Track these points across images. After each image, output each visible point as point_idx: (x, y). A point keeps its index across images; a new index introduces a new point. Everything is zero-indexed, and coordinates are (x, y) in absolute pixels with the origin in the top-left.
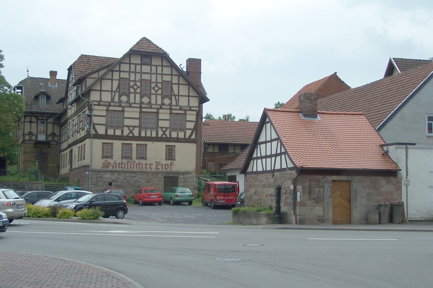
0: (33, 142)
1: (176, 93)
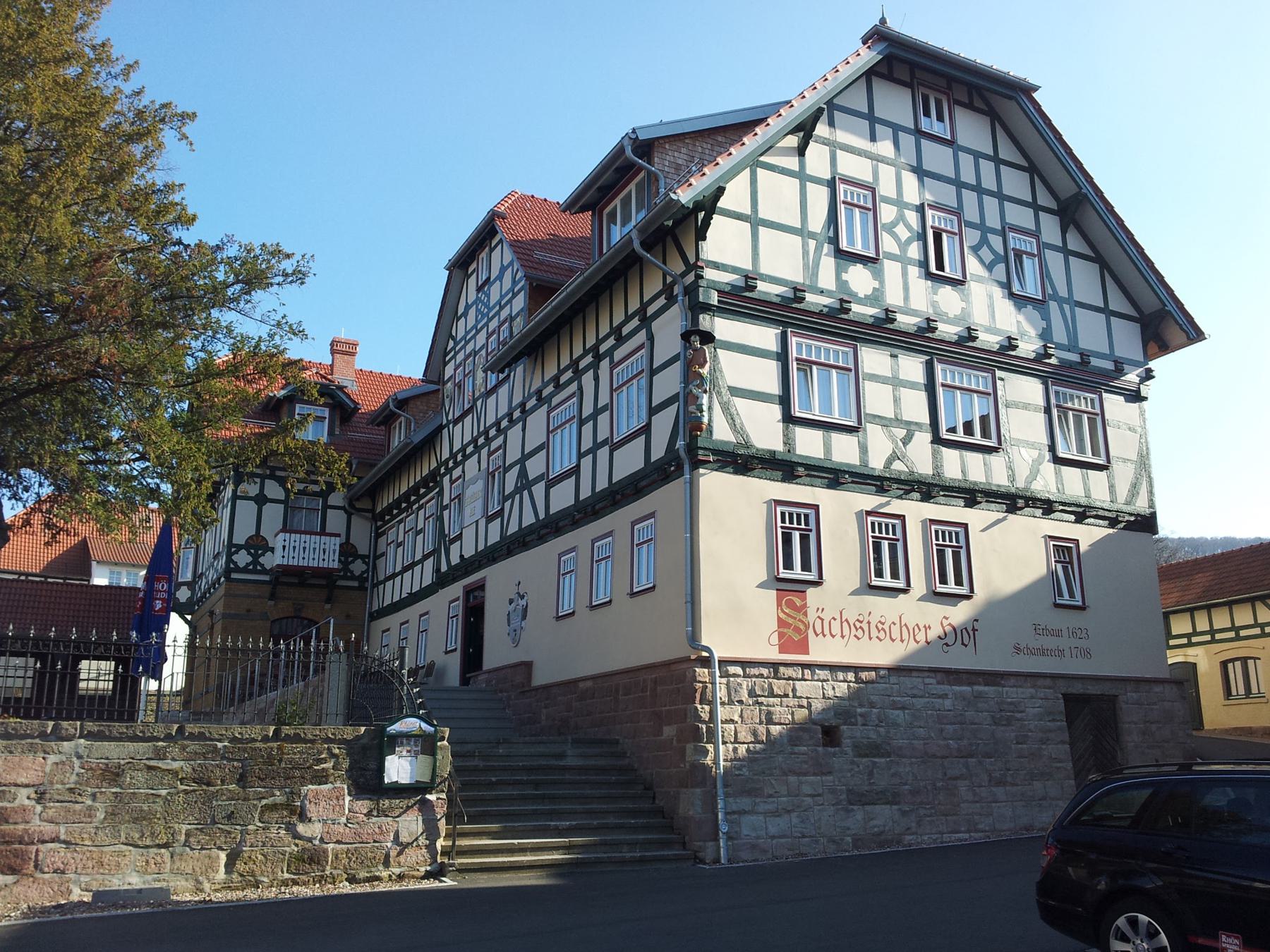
0: (267, 578)
1: (1063, 292)
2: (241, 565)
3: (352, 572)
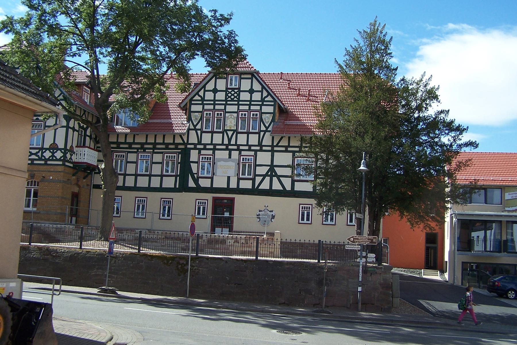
0: (71, 165)
2: (58, 158)
3: (55, 157)
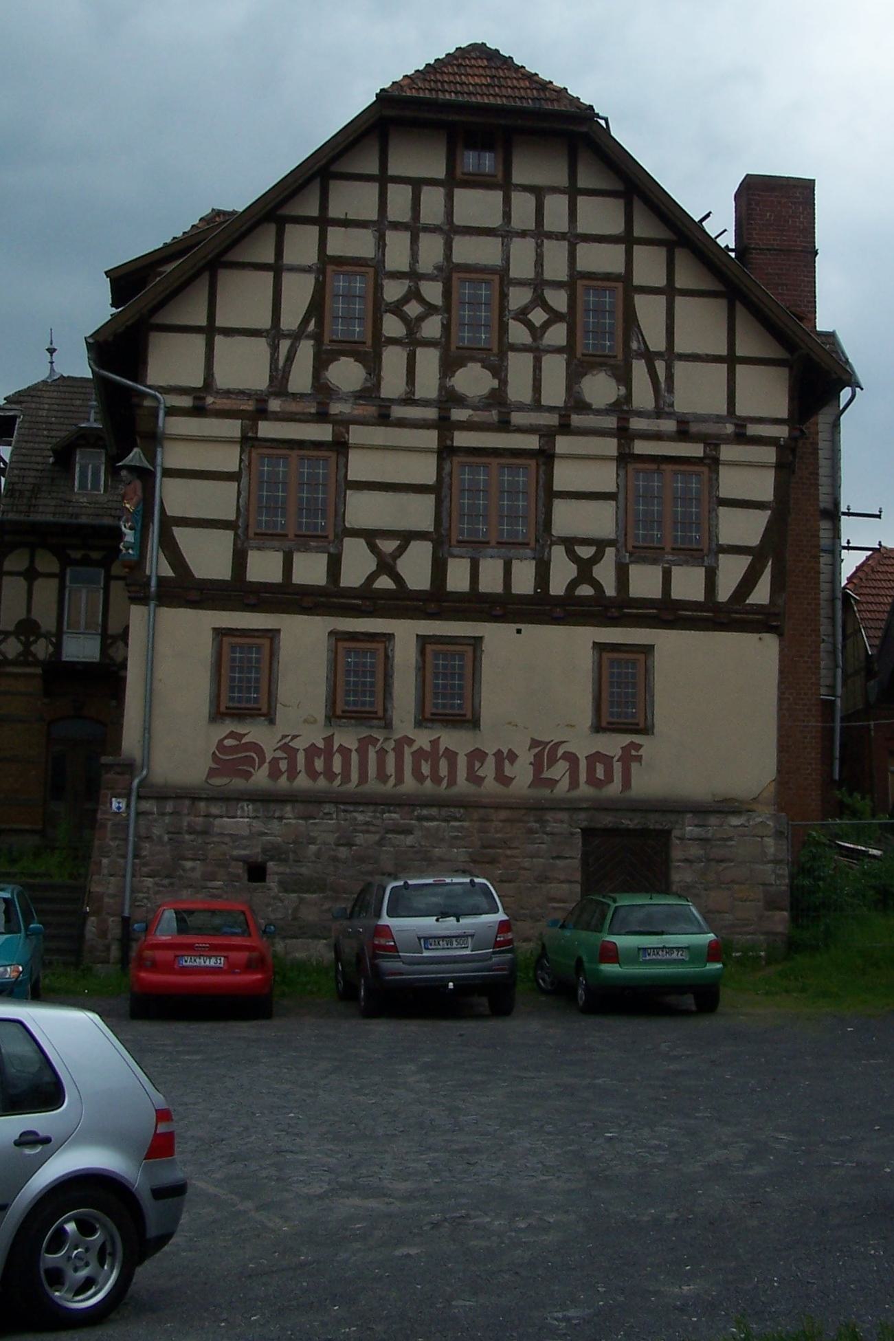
0: (39, 671)
1: (657, 343)
3: (34, 656)
